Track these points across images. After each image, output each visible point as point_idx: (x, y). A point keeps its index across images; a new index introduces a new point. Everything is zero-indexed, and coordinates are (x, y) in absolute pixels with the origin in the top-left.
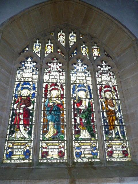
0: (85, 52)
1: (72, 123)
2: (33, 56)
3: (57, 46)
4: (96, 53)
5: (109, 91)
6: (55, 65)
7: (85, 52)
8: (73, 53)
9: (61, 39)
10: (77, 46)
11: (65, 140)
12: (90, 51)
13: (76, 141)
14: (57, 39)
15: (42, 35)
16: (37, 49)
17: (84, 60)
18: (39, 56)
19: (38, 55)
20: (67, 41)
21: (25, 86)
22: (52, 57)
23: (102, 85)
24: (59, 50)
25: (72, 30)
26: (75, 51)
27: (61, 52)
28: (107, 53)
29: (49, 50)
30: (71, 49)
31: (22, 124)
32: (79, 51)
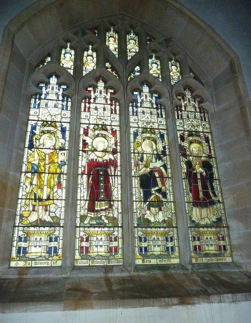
0: (154, 69)
1: (78, 171)
2: (60, 73)
3: (104, 56)
4: (175, 72)
5: (195, 141)
6: (100, 94)
7: (154, 69)
8: (133, 71)
9: (112, 44)
10: (141, 60)
11: (120, 227)
12: (165, 70)
13: (139, 229)
14: (59, 62)
15: (76, 34)
16: (67, 60)
17: (154, 85)
18: (72, 73)
19: (69, 71)
20: (79, 63)
21: (46, 128)
22: (96, 77)
23: (139, 127)
24: (107, 64)
25: (132, 27)
26: (138, 68)
27: (113, 68)
28: (194, 73)
29: (90, 64)
30: (146, 58)
31: (178, 303)
32: (145, 68)
